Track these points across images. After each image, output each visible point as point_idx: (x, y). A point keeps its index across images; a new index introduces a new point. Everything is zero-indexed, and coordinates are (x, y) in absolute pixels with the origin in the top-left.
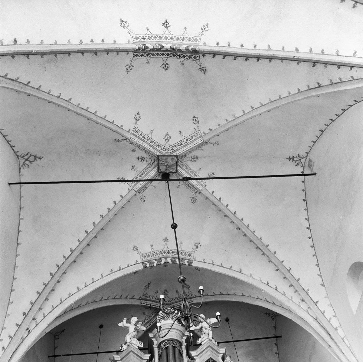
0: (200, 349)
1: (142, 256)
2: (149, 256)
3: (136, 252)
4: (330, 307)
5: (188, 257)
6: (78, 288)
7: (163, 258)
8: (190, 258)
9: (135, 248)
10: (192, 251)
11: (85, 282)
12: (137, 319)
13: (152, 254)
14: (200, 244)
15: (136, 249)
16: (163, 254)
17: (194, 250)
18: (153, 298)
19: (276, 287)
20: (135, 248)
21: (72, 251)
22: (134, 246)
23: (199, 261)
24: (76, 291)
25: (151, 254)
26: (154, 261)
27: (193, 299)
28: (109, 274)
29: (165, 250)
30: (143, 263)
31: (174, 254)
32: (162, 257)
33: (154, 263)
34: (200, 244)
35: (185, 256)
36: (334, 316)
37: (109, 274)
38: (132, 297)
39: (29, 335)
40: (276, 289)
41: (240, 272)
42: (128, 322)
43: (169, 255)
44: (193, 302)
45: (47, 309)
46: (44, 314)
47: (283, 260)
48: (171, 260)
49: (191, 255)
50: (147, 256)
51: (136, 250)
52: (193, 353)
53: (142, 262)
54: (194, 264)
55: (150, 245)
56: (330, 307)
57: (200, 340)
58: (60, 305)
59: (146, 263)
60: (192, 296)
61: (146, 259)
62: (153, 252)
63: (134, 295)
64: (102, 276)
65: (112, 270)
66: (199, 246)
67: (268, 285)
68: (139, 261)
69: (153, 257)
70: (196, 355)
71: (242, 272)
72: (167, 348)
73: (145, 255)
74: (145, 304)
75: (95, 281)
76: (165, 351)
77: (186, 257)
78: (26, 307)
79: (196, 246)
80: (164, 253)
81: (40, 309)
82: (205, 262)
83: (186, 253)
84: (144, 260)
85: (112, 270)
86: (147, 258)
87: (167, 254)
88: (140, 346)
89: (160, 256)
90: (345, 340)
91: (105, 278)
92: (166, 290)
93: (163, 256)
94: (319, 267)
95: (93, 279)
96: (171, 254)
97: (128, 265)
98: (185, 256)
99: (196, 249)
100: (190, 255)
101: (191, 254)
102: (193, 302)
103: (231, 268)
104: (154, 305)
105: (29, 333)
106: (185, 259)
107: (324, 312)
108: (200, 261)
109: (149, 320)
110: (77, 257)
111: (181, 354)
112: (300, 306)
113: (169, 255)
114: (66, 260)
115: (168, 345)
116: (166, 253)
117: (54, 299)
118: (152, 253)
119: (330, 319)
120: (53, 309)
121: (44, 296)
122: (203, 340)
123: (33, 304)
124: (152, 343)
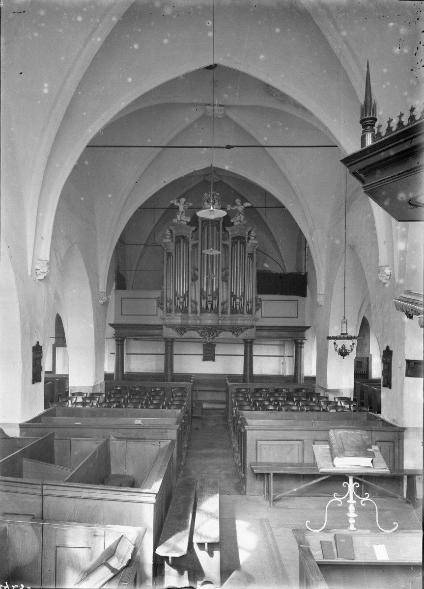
42: (179, 202)
52: (228, 229)
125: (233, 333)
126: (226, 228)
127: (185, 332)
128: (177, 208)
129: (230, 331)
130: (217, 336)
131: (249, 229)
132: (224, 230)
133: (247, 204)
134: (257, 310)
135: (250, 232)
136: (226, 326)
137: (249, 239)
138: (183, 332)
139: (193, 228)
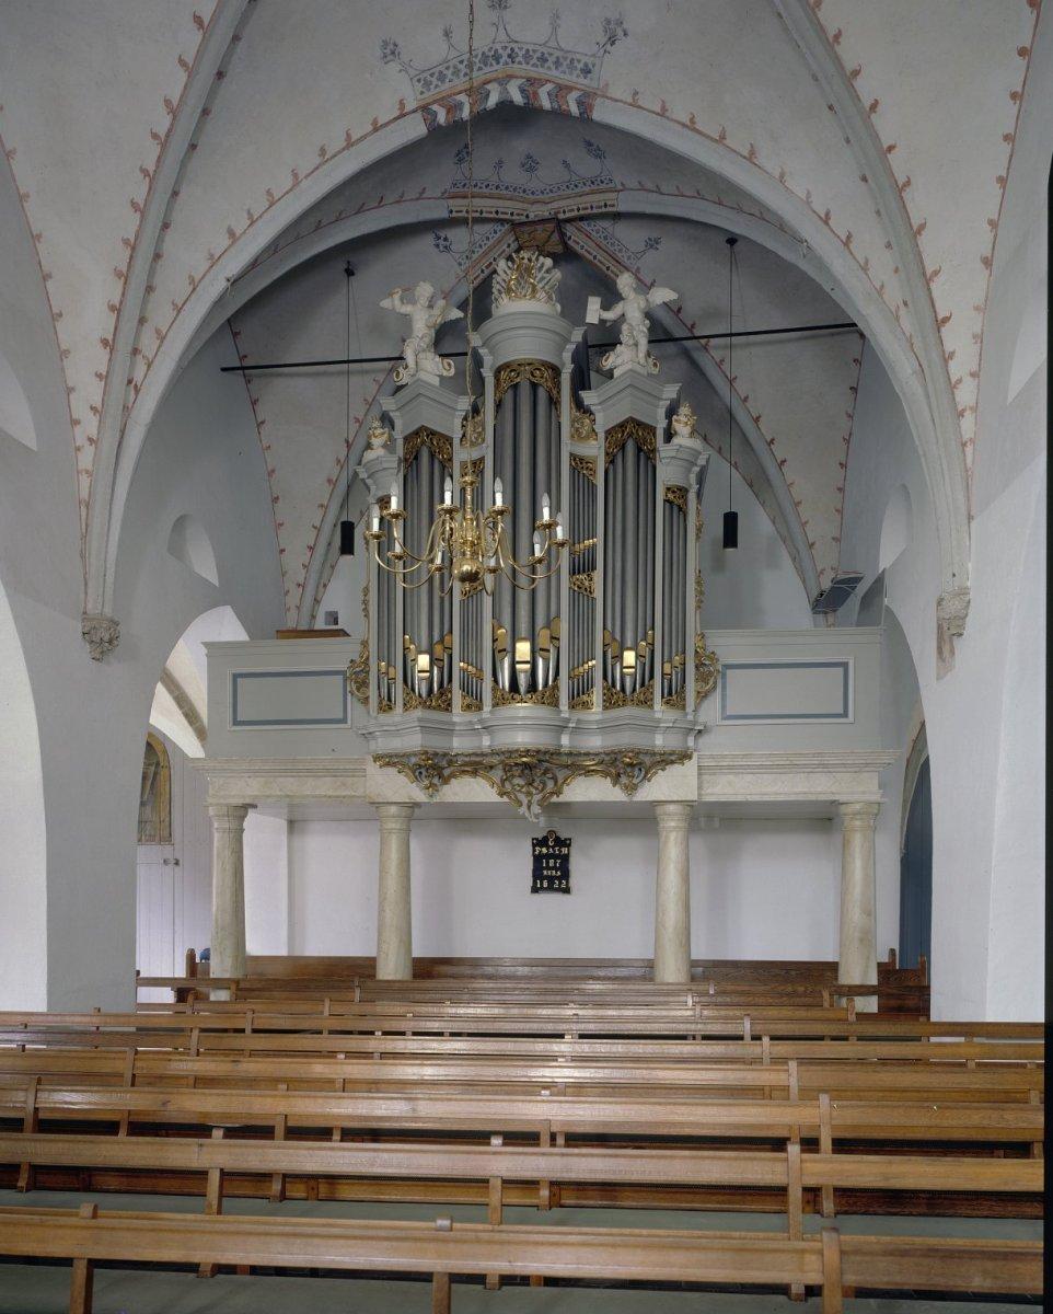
0: (610, 388)
1: (419, 81)
2: (442, 77)
3: (394, 67)
4: (976, 343)
5: (582, 80)
6: (231, 233)
7: (495, 80)
8: (586, 82)
9: (391, 51)
10: (593, 55)
11: (246, 208)
12: (432, 289)
13: (451, 70)
14: (625, 26)
15: (393, 53)
16: (491, 65)
17: (602, 51)
18: (487, 186)
19: (849, 237)
20: (391, 51)
21: (174, 113)
22: (385, 44)
23: (617, 101)
24: (227, 242)
25: (447, 68)
26: (458, 97)
27: (614, 195)
28: (317, 168)
29: (498, 46)
30: (425, 108)
31: (532, 62)
32: (488, 76)
33: (460, 106)
34: (625, 26)
35: (571, 74)
36: (973, 375)
37: (317, 168)
38: (418, 195)
39: (139, 397)
40: (847, 243)
41: (751, 157)
43: (515, 68)
44: (613, 206)
45: (161, 315)
46: (158, 332)
47: (891, 142)
48: (522, 91)
49: (589, 72)
50: (434, 80)
51: (391, 57)
53: (421, 103)
54: (598, 115)
55: (440, 33)
56: (976, 343)
57: (610, 360)
58: (193, 296)
59: (435, 107)
60: (610, 185)
61: (433, 91)
62: (455, 61)
63: (424, 189)
64: (295, 175)
65: (323, 151)
66: (620, 33)
67: (826, 223)
68: (411, 105)
69: (456, 81)
70: (597, 402)
71: (755, 160)
72: (515, 387)
73: (426, 74)
74: (461, 211)
75: (276, 198)
76: (510, 392)
77: (574, 79)
78: (103, 324)
79: (608, 36)
80: (497, 58)
81: (142, 321)
82: (640, 103)
83: (572, 61)
84: (429, 96)
85: (323, 151)
86: (437, 86)
87: (507, 64)
88: (445, 374)
89: (481, 73)
90: (969, 449)
91: (305, 183)
92: (529, 157)
93: (494, 75)
94: (1004, 188)
95: (269, 192)
96: (520, 63)
97: (375, 122)
98: (571, 74)
99: (608, 46)
100: (587, 71)
101: (591, 66)
102: (613, 206)
103: (723, 137)
104: (494, 210)
105: (137, 390)
106: (570, 89)
107: (952, 355)
108: (621, 101)
109: (484, 248)
110: (176, 183)
111: (554, 402)
112: (897, 318)
113: (515, 68)
114: (164, 146)
115: (518, 380)
116: (502, 61)
117: (172, 283)
118: (451, 64)
119: (960, 381)
120: (179, 312)
121: (124, 347)
122: (619, 361)
123: (119, 311)
124: (478, 362)
125: (616, 779)
126: (583, 394)
127: (446, 781)
128: (406, 320)
129: (606, 774)
130: (558, 793)
131: (671, 391)
132: (579, 404)
133: (662, 295)
134: (702, 696)
135: (671, 412)
136: (587, 754)
137: (669, 435)
138: (436, 780)
139: (464, 404)
